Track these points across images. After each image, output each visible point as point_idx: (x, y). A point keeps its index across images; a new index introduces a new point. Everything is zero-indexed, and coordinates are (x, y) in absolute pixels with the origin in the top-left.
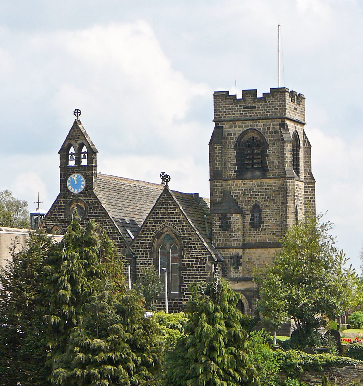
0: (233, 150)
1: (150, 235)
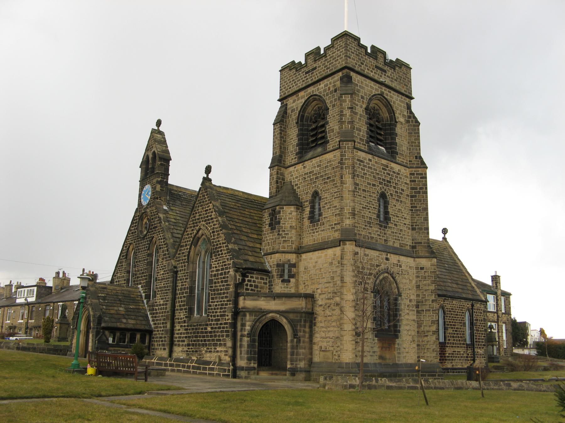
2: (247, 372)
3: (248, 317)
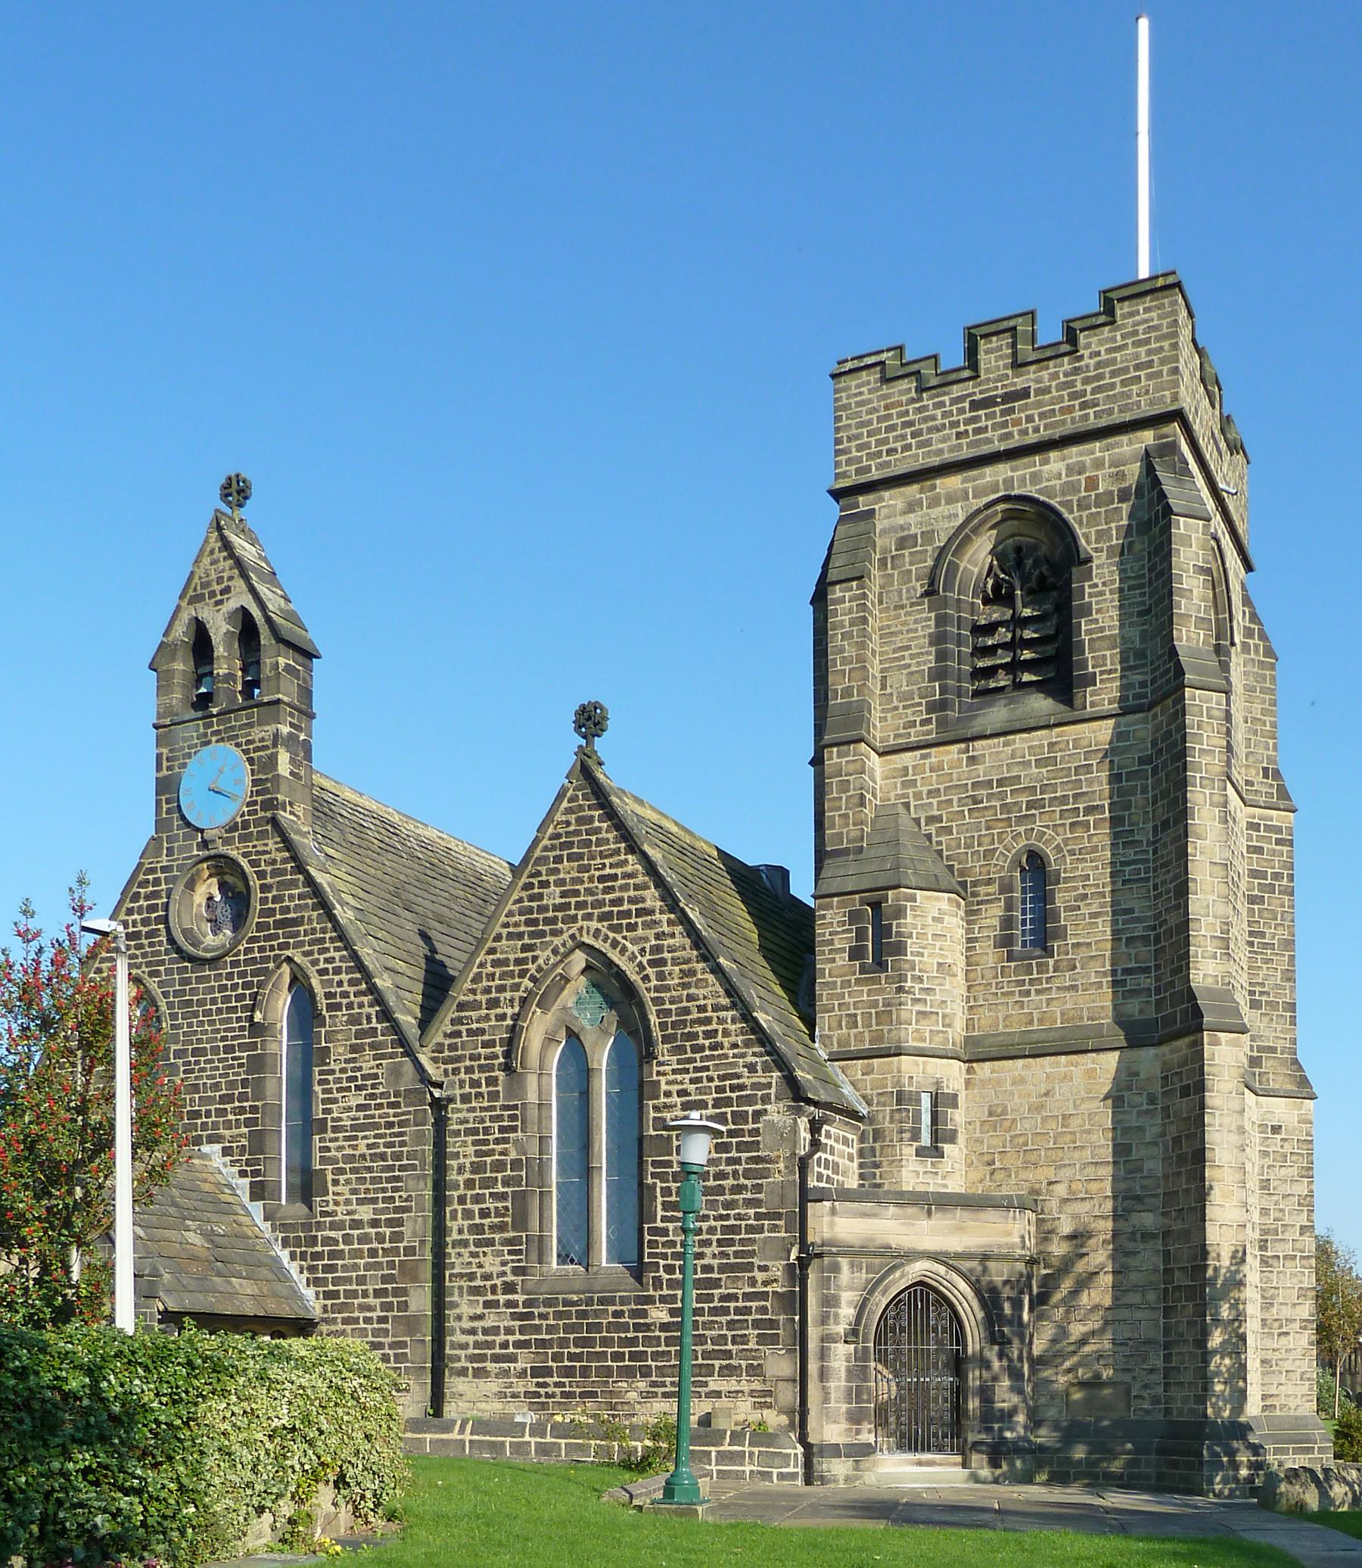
0: (922, 611)
1: (508, 995)
2: (850, 1462)
3: (845, 1275)
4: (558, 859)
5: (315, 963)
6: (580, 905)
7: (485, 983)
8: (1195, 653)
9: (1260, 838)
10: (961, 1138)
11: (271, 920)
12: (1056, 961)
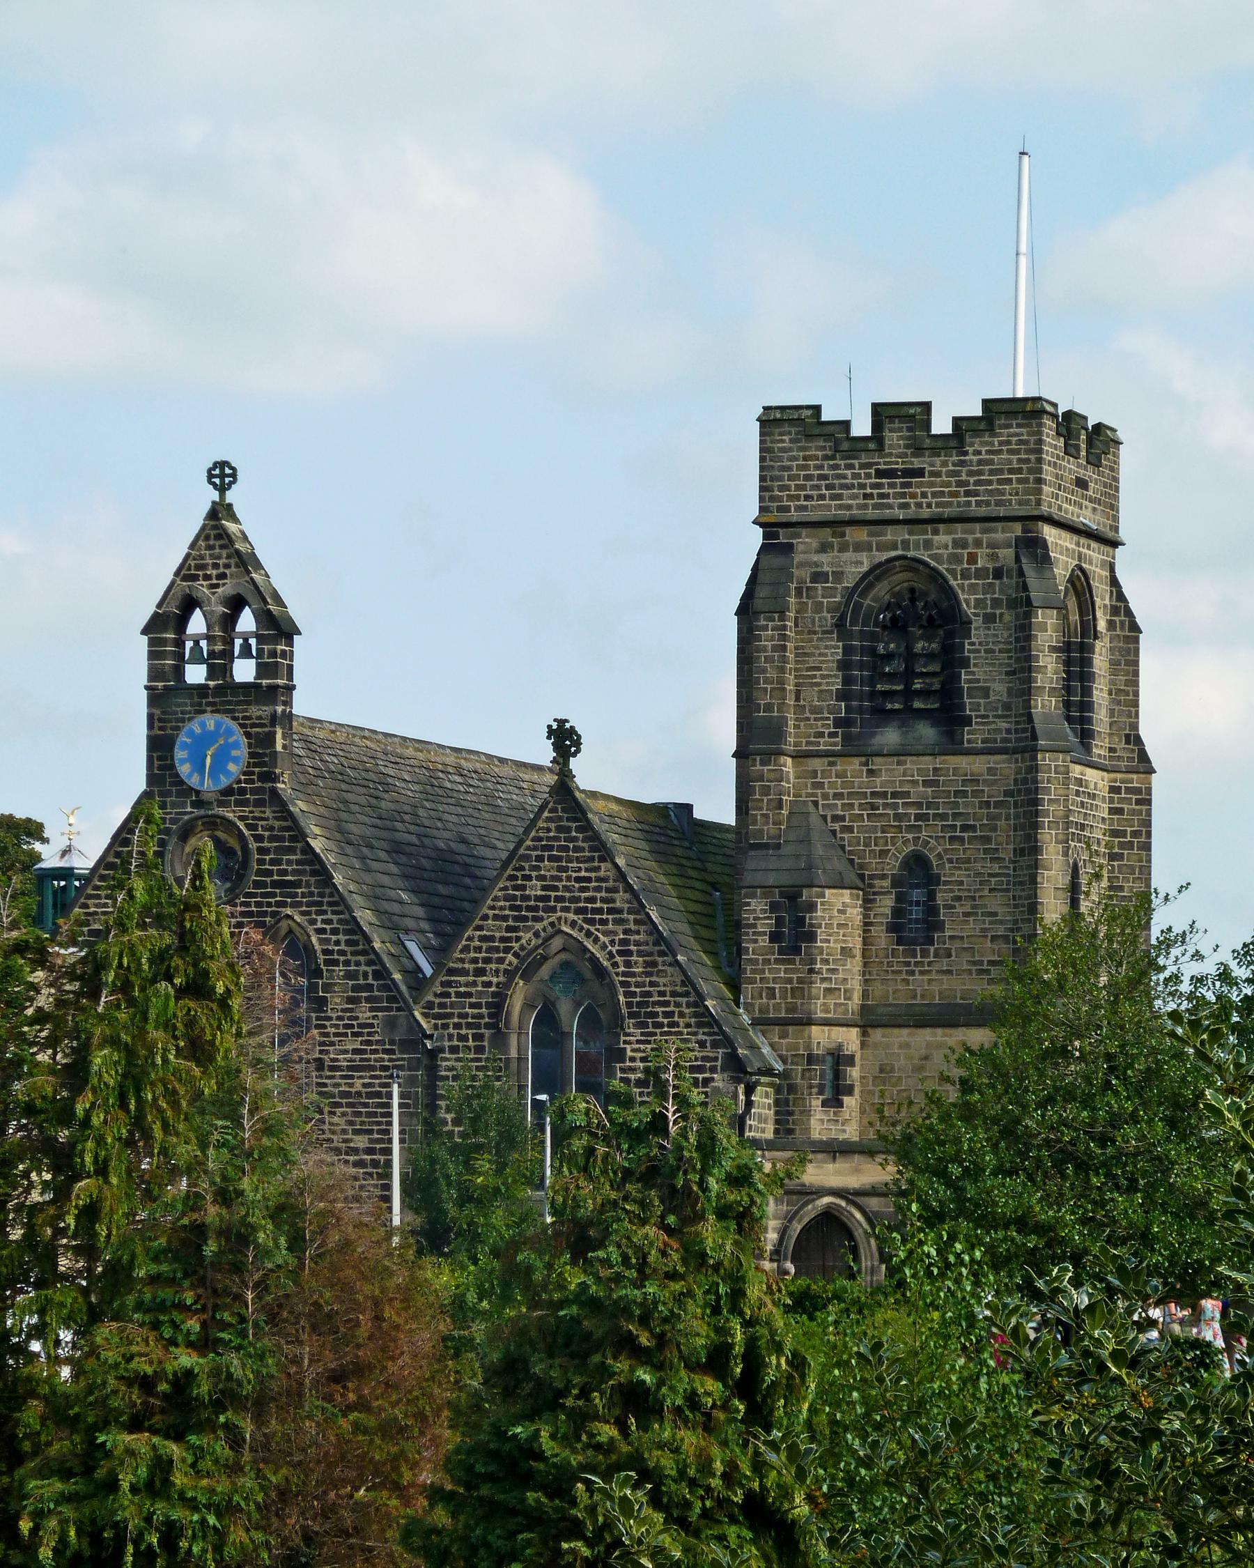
0: (831, 639)
1: (494, 966)
4: (540, 859)
5: (313, 922)
6: (559, 899)
7: (472, 955)
8: (1047, 717)
9: (1121, 800)
10: (857, 1090)
11: (268, 879)
12: (936, 950)
